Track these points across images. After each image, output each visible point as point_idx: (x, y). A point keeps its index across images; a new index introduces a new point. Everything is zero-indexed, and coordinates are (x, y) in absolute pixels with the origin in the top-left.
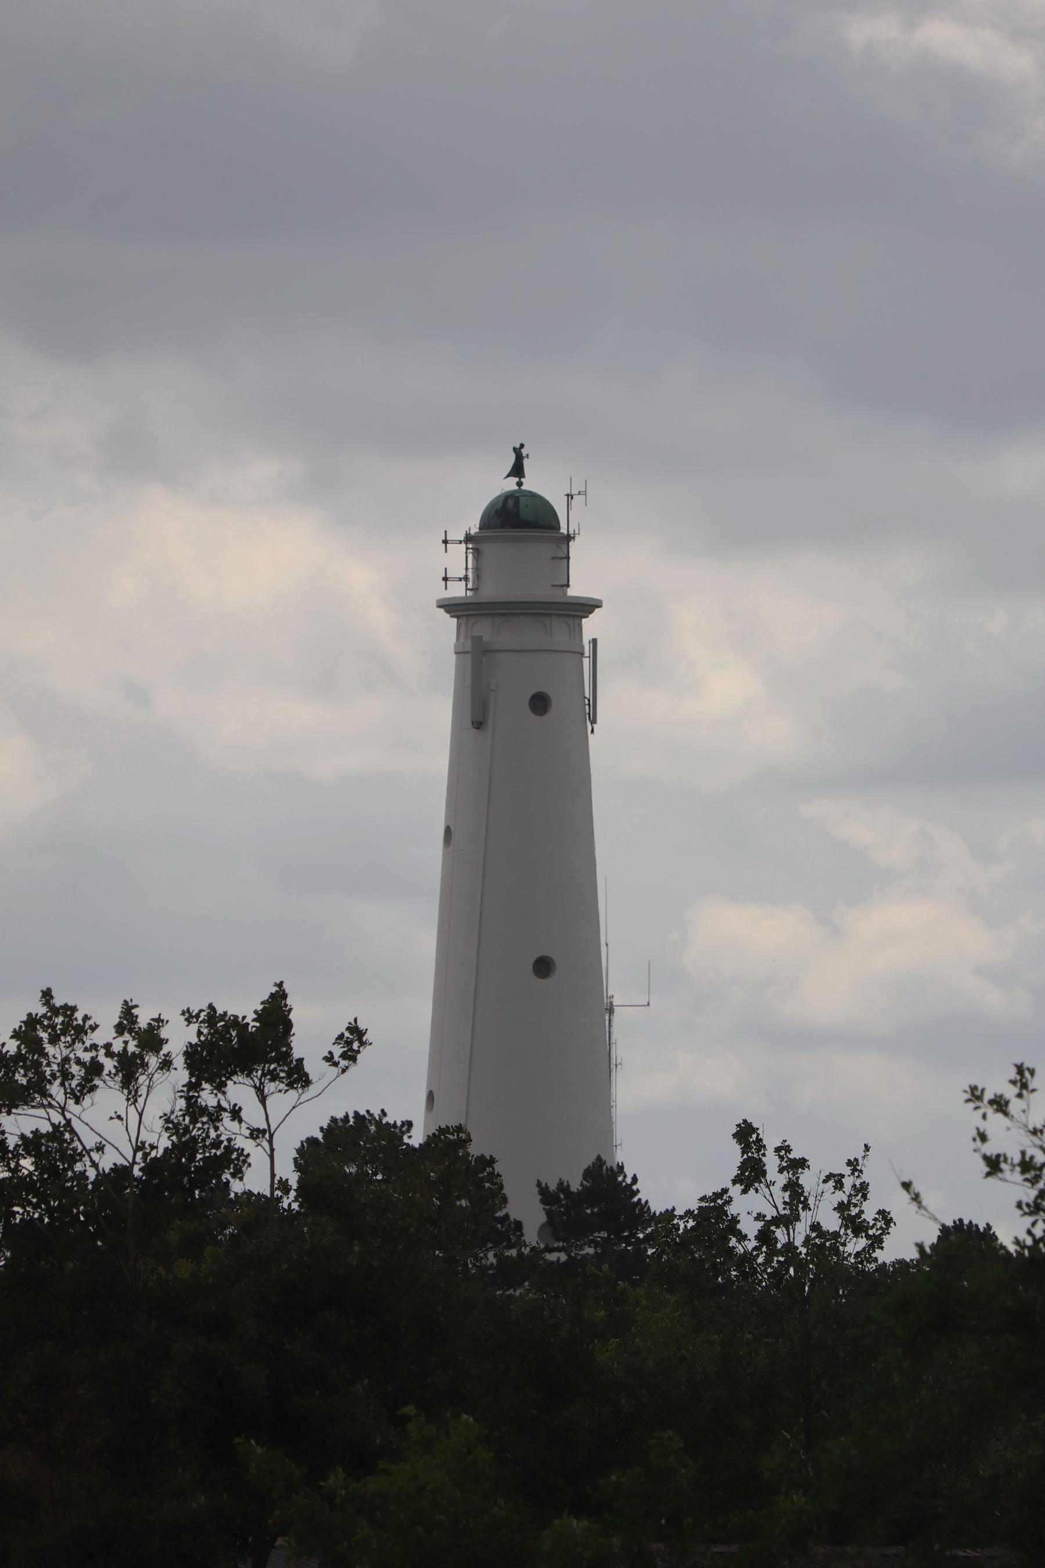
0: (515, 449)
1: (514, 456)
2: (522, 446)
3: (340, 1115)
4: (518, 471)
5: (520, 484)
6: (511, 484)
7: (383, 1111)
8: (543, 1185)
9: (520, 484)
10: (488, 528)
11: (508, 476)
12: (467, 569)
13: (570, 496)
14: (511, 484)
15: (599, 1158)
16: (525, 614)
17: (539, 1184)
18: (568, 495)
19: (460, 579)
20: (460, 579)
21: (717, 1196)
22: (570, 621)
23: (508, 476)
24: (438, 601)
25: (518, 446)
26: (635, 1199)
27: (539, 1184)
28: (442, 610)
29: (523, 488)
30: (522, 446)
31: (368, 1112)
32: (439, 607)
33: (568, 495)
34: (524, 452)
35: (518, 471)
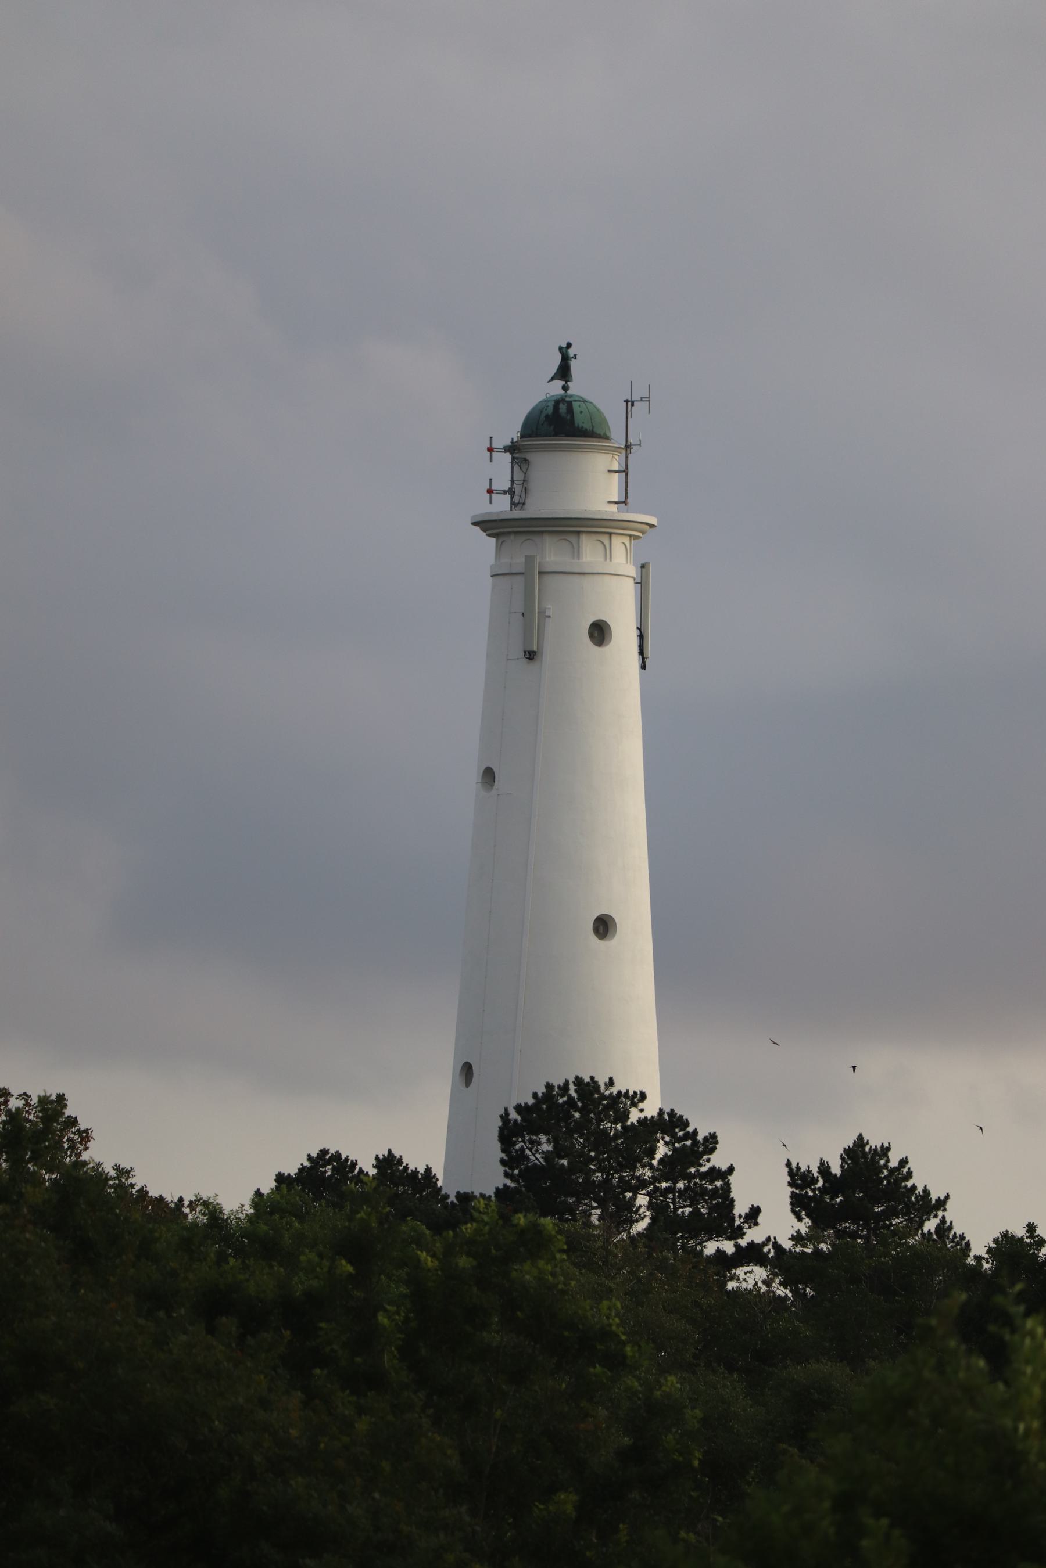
0: (561, 349)
1: (560, 356)
2: (569, 345)
3: (557, 1081)
4: (564, 372)
5: (565, 388)
6: (556, 389)
7: (611, 1079)
8: (794, 1166)
9: (565, 388)
10: (530, 436)
11: (552, 379)
12: (512, 481)
13: (629, 403)
14: (556, 389)
15: (860, 1137)
16: (516, 533)
17: (789, 1164)
18: (627, 401)
19: (505, 492)
20: (505, 492)
21: (791, 1173)
22: (573, 539)
23: (552, 379)
24: (473, 517)
25: (564, 346)
26: (909, 1184)
27: (789, 1164)
28: (477, 528)
29: (569, 392)
30: (569, 345)
31: (592, 1078)
32: (475, 524)
33: (627, 401)
34: (571, 352)
35: (564, 372)
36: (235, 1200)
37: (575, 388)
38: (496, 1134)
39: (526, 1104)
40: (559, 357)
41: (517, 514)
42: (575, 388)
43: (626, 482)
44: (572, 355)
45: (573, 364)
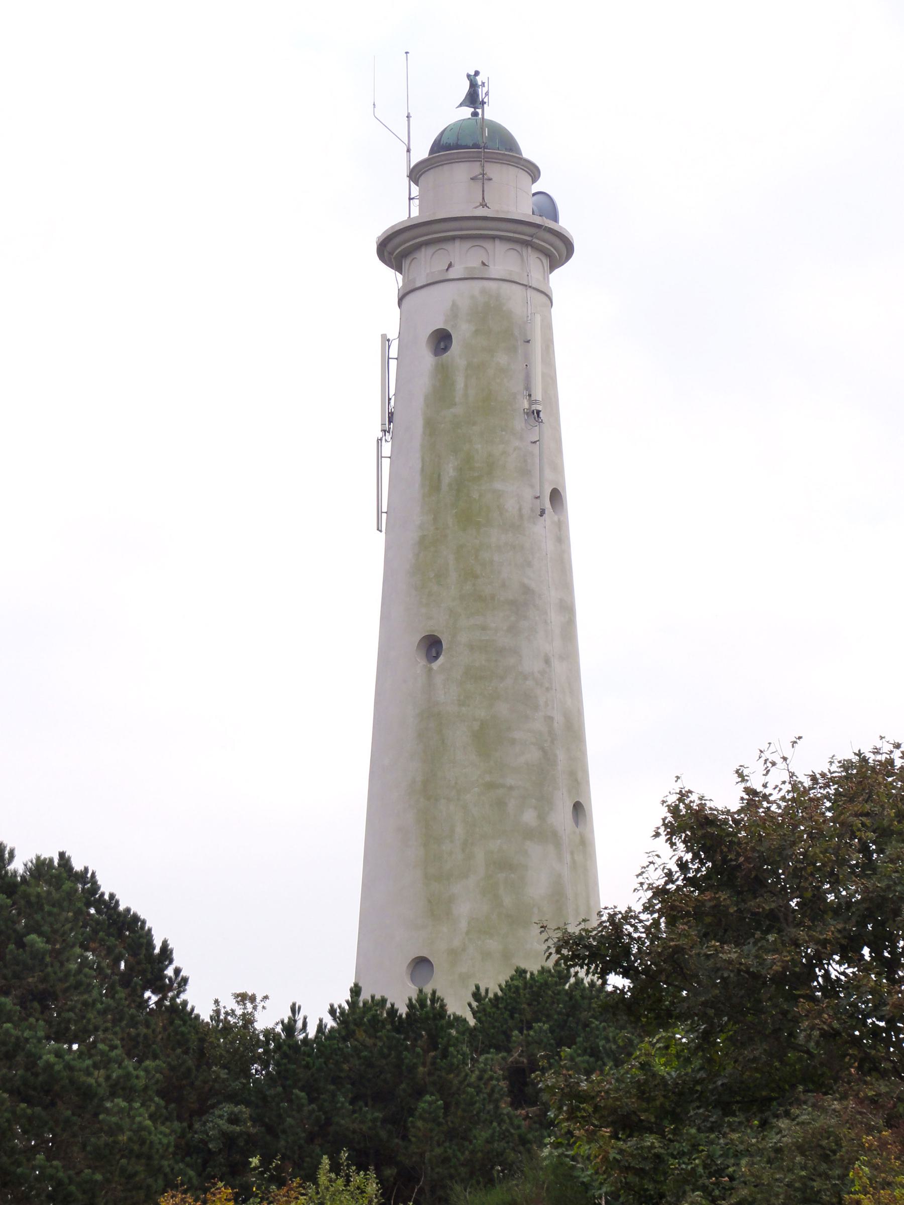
0: (468, 76)
2: (477, 73)
4: (473, 99)
11: (461, 105)
23: (461, 105)
25: (473, 73)
28: (527, 153)
30: (477, 73)
34: (479, 79)
35: (473, 99)
36: (202, 1000)
37: (491, 113)
38: (123, 884)
39: (198, 1016)
40: (467, 84)
41: (481, 212)
42: (491, 113)
43: (482, 279)
44: (480, 83)
45: (481, 92)
